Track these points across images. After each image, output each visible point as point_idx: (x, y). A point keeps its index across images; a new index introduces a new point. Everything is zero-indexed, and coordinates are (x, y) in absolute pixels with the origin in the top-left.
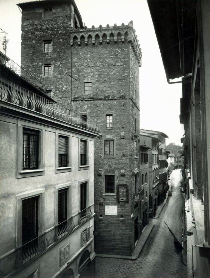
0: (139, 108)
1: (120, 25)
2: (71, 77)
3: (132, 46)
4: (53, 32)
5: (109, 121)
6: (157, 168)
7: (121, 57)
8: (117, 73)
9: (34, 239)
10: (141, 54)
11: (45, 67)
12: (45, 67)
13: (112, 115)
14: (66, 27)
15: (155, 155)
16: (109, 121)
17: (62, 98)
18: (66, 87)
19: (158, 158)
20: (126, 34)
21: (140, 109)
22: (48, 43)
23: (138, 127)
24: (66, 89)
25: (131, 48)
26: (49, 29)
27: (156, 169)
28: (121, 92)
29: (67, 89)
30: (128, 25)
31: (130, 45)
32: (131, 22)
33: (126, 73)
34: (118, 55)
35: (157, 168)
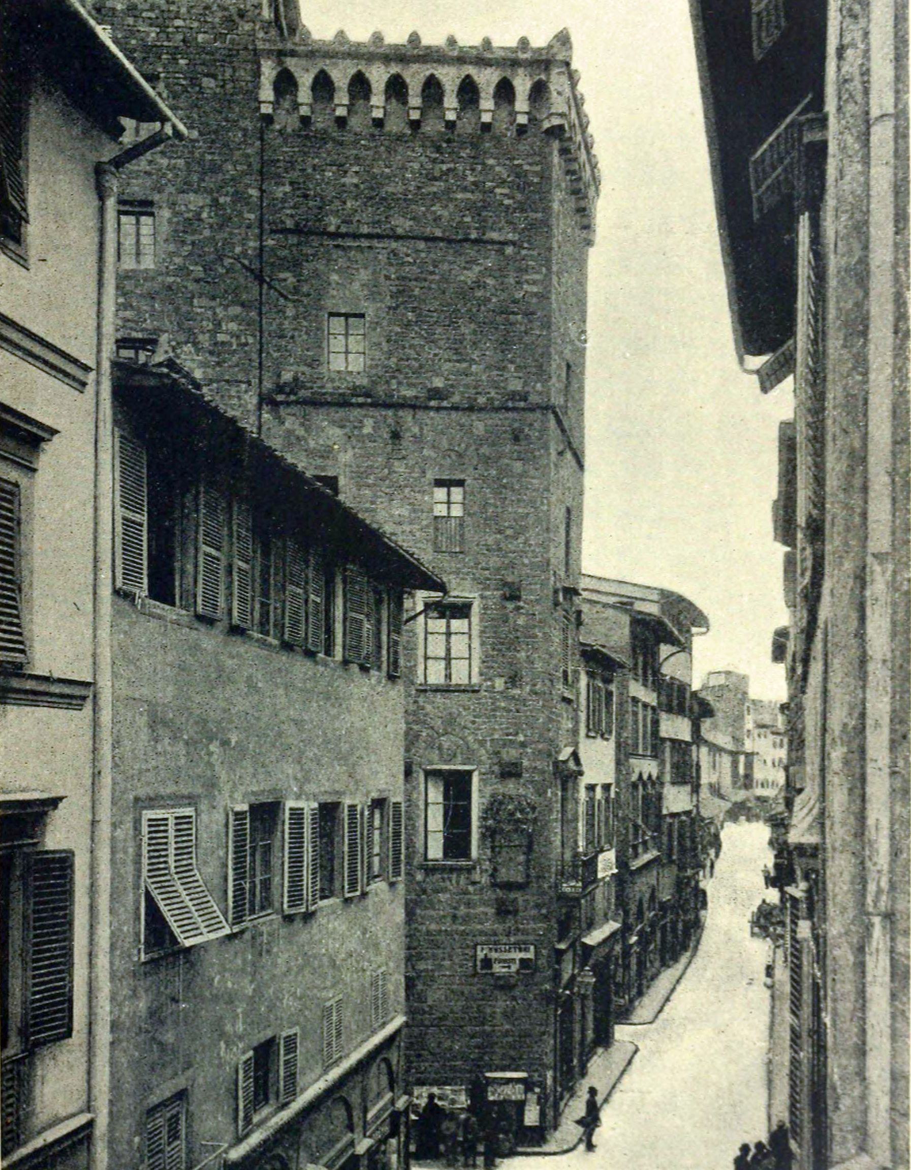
0: (583, 456)
1: (513, 43)
2: (261, 281)
3: (564, 151)
4: (163, 35)
5: (448, 626)
6: (650, 777)
7: (511, 201)
8: (490, 281)
9: (120, 55)
10: (596, 181)
11: (120, 213)
12: (120, 213)
13: (460, 483)
14: (236, 18)
15: (645, 706)
16: (448, 626)
17: (215, 385)
18: (233, 326)
19: (656, 723)
20: (539, 91)
21: (588, 461)
22: (138, 215)
23: (544, 52)
24: (234, 340)
25: (556, 159)
26: (144, 15)
27: (645, 777)
28: (506, 375)
29: (238, 337)
30: (550, 47)
31: (556, 145)
32: (563, 39)
33: (535, 283)
34: (498, 191)
35: (650, 777)
